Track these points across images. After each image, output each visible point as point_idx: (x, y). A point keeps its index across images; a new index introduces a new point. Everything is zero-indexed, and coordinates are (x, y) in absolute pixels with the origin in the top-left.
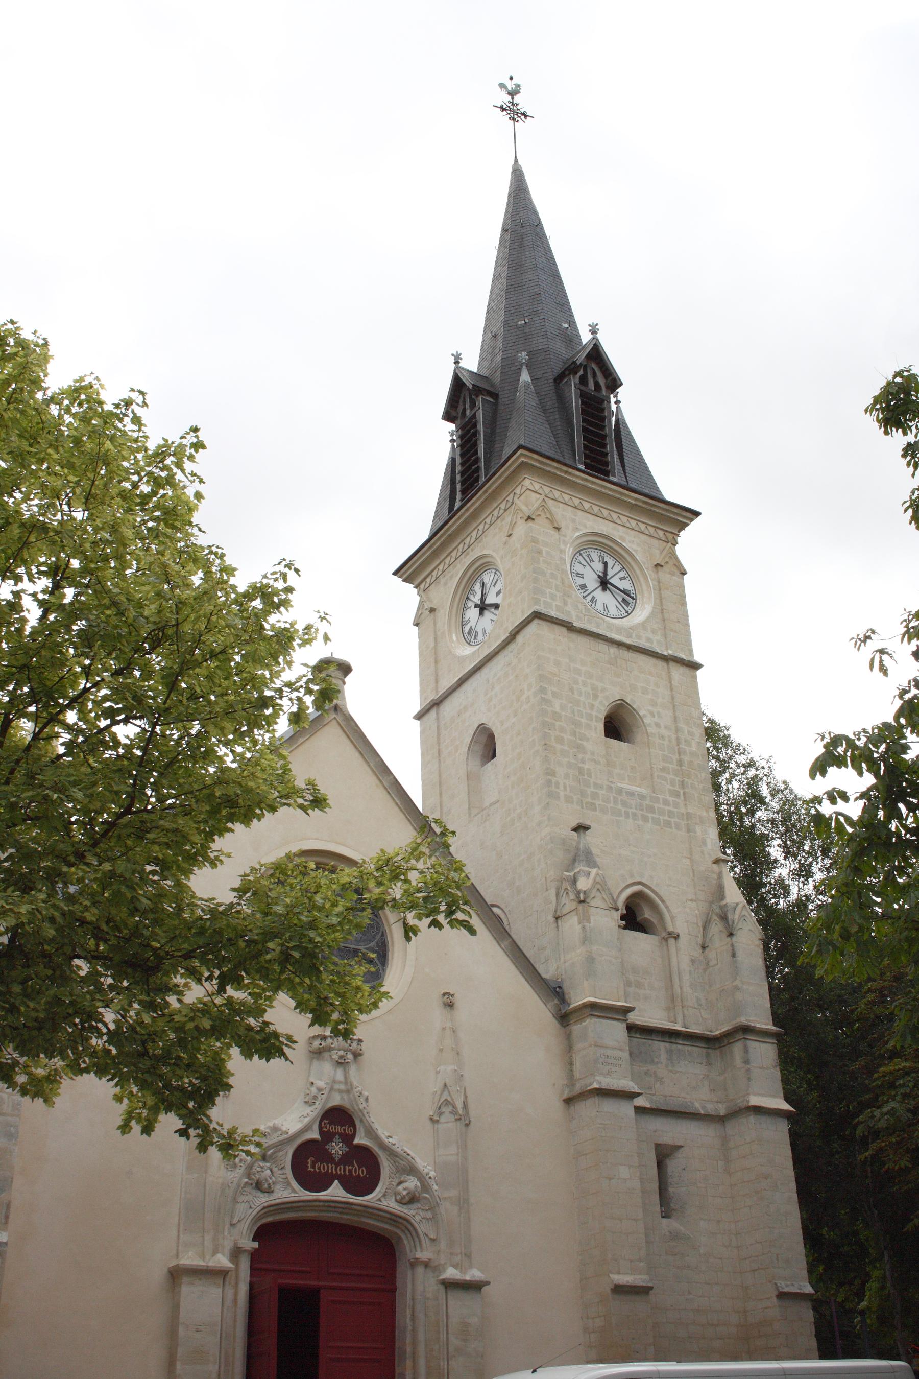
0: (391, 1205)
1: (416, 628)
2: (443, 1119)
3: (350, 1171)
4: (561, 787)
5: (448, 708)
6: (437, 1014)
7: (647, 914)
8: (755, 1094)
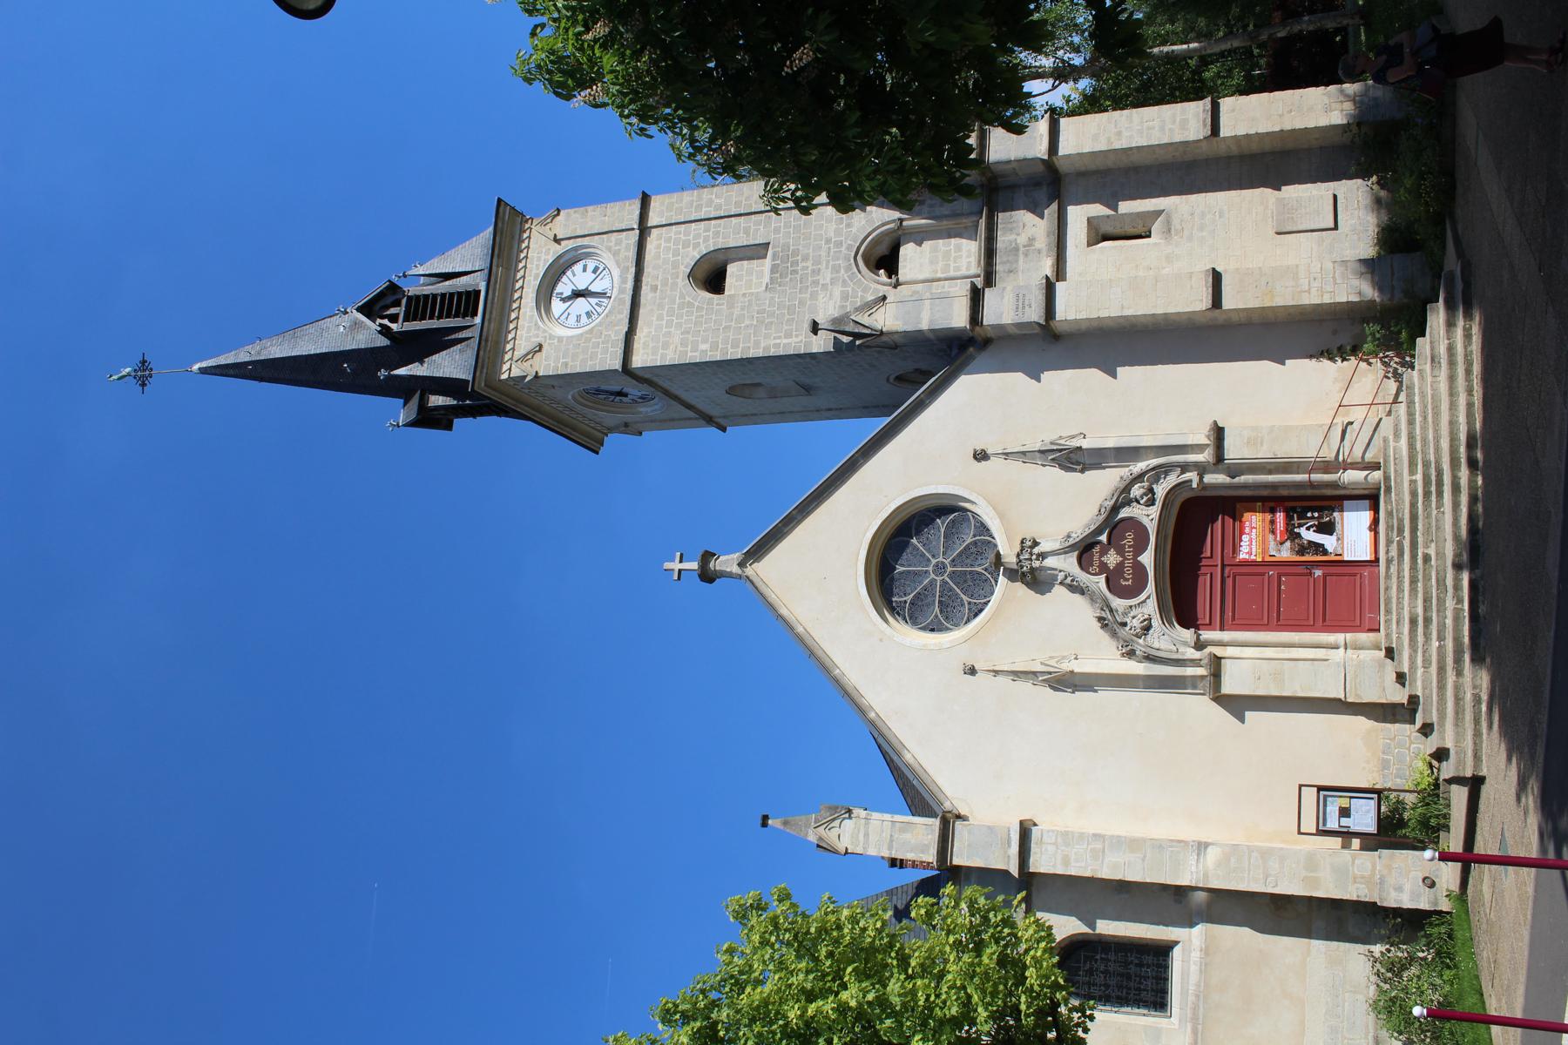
0: (1154, 511)
6: (994, 463)
7: (883, 249)
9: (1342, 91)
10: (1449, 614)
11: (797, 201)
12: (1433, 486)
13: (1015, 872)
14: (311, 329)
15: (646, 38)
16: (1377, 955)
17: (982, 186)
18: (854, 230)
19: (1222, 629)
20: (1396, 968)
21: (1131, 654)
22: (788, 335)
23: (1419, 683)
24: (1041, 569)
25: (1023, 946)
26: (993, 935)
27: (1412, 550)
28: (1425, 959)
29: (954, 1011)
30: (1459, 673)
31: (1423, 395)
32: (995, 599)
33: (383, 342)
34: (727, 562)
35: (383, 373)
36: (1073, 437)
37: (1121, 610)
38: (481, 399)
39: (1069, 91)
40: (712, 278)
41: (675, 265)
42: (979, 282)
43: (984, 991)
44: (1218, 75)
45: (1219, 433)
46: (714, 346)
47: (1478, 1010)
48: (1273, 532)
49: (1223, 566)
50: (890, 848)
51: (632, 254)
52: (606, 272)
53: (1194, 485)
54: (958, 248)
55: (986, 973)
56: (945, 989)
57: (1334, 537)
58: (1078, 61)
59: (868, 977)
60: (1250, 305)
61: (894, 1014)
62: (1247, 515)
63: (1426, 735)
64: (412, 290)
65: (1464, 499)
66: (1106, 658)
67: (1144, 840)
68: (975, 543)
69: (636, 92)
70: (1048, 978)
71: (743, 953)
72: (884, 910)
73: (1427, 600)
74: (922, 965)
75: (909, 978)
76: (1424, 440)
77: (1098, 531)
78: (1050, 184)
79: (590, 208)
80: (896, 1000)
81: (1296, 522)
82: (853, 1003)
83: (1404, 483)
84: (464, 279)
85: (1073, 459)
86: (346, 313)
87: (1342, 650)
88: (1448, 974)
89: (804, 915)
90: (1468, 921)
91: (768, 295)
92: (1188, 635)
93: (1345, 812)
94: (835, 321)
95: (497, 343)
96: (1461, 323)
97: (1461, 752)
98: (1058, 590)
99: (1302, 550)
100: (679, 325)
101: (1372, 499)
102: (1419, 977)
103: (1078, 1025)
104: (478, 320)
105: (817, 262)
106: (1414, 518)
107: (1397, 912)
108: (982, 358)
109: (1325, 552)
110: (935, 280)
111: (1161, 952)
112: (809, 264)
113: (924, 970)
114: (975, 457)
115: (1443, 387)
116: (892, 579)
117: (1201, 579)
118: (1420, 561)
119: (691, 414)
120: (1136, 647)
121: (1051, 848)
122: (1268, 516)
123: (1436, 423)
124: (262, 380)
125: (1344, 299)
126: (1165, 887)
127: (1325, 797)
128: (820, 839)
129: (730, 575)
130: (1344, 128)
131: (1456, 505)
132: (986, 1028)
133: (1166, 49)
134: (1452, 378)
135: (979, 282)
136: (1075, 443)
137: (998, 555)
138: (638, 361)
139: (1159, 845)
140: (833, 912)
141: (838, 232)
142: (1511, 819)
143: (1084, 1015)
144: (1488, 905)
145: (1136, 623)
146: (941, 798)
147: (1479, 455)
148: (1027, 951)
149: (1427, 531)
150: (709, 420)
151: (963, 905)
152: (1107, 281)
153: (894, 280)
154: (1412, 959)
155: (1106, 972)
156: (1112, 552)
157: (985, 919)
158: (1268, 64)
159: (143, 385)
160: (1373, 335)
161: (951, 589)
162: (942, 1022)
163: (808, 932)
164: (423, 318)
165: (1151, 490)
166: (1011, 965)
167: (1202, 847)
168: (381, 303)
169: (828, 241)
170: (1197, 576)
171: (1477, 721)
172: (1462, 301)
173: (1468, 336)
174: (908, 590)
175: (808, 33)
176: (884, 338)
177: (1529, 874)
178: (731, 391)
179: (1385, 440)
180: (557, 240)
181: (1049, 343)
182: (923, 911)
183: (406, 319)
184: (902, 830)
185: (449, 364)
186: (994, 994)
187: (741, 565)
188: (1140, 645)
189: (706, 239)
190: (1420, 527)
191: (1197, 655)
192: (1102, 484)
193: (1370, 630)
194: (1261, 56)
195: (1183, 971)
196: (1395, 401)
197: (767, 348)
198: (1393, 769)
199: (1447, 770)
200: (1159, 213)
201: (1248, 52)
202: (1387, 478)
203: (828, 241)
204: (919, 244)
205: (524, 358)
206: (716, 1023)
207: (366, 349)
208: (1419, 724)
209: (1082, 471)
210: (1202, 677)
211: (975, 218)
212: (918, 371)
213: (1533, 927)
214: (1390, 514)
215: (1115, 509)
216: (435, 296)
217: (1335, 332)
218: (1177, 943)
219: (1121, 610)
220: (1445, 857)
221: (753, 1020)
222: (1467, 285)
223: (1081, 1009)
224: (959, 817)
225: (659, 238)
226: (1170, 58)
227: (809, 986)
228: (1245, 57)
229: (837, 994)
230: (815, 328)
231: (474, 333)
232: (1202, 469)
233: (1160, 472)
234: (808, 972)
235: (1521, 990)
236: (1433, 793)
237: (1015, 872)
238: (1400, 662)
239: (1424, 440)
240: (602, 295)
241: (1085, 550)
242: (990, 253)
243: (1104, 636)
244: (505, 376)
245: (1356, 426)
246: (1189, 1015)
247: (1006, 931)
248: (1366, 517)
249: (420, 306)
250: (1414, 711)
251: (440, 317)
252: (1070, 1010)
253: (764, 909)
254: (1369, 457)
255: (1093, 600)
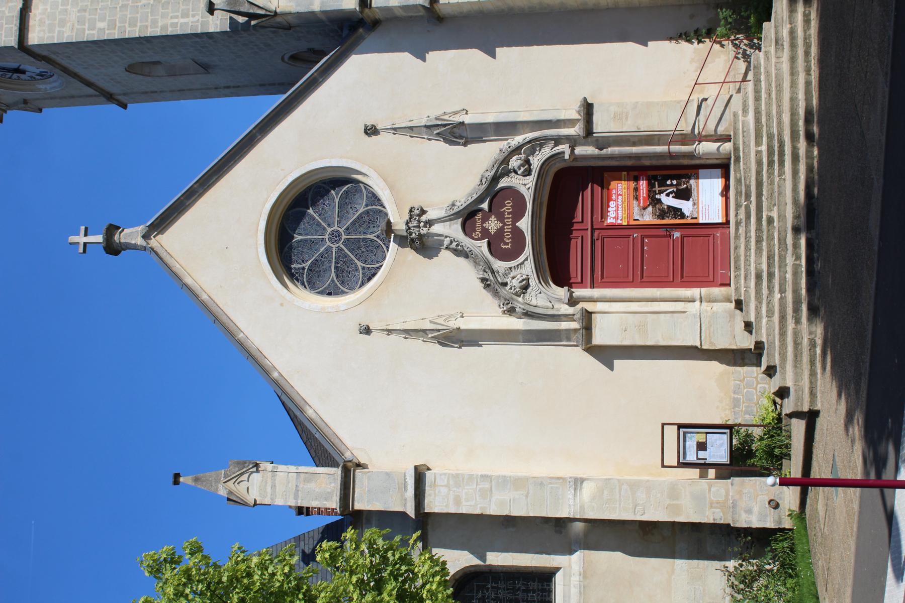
0: (531, 181)
1: (43, 110)
2: (464, 134)
3: (509, 214)
4: (176, 21)
6: (383, 138)
8: (576, 330)
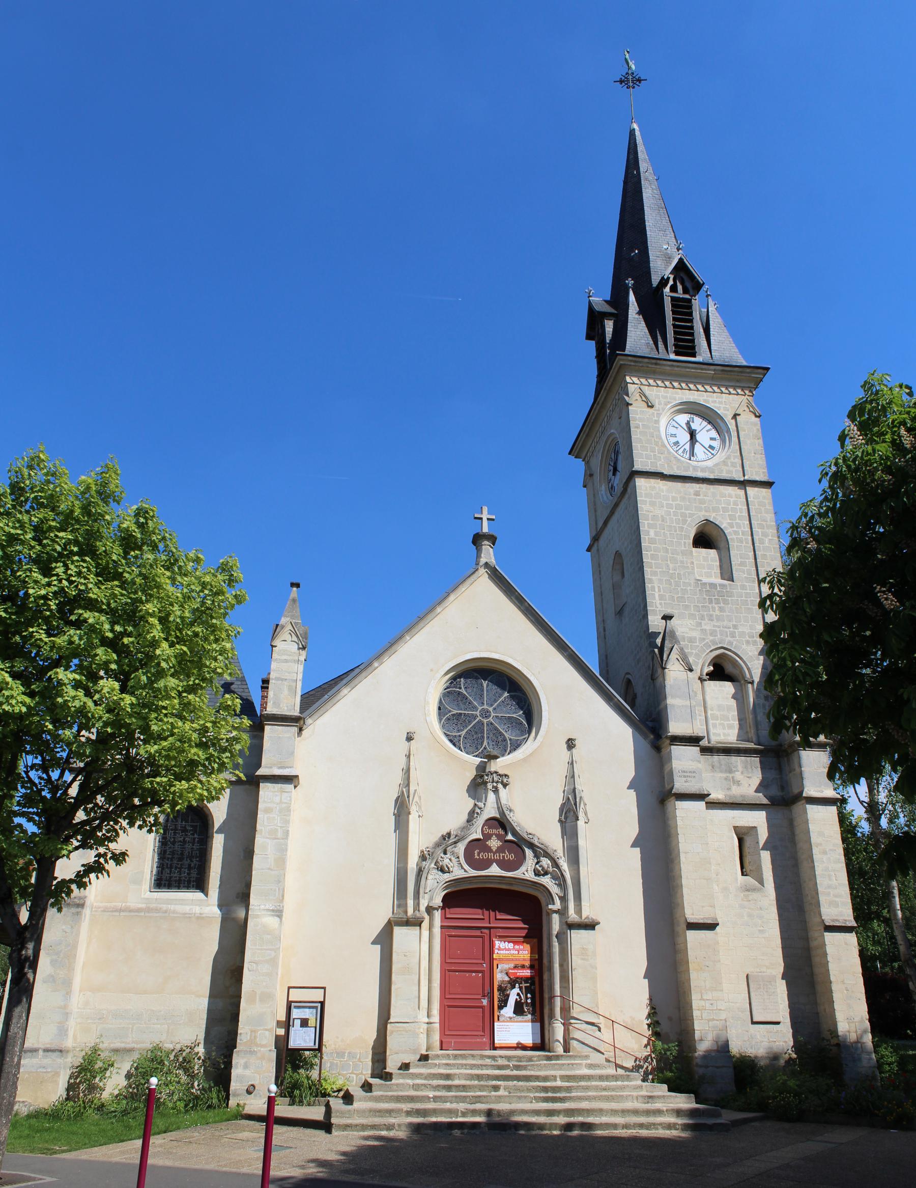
0: (530, 876)
5: (602, 541)
6: (565, 754)
7: (729, 669)
9: (865, 1032)
10: (454, 1106)
11: (770, 597)
12: (552, 1094)
13: (260, 772)
14: (665, 222)
15: (900, 475)
16: (196, 1050)
17: (781, 745)
18: (744, 646)
19: (442, 927)
20: (185, 1065)
21: (423, 858)
22: (661, 597)
23: (401, 1081)
24: (486, 790)
25: (204, 779)
26: (212, 756)
27: (500, 1077)
28: (193, 1087)
29: (154, 728)
30: (409, 1113)
31: (622, 1088)
32: (463, 755)
33: (655, 280)
34: (488, 554)
35: (630, 282)
36: (586, 814)
37: (456, 850)
38: (610, 360)
39: (857, 811)
40: (706, 538)
41: (715, 510)
42: (704, 743)
43: (170, 749)
44: (875, 934)
45: (590, 926)
46: (652, 541)
47: (154, 1129)
48: (516, 967)
49: (490, 928)
50: (277, 679)
51: (724, 475)
52: (711, 456)
53: (550, 907)
54: (730, 727)
55: (183, 751)
56: (171, 720)
57: (511, 1014)
58: (884, 822)
59: (180, 663)
60: (690, 953)
61: (151, 682)
62: (528, 947)
63: (363, 1087)
64: (696, 303)
65: (542, 1119)
66: (420, 838)
67: (284, 869)
68: (505, 740)
69: (857, 470)
70: (181, 797)
71: (196, 569)
72: (230, 674)
73: (464, 1088)
74: (189, 703)
75: (180, 694)
76: (587, 1088)
77: (515, 833)
78: (783, 798)
79: (761, 441)
80: (161, 684)
81: (524, 985)
82: (158, 652)
83: (553, 1071)
84: (704, 343)
85: (569, 814)
86: (678, 249)
87: (427, 1020)
88: (181, 1105)
89: (225, 614)
90: (221, 1121)
91: (692, 582)
92: (438, 901)
93: (304, 1023)
94: (673, 633)
95: (654, 372)
96: (680, 1121)
97: (350, 1114)
98: (470, 803)
99: (501, 989)
100: (669, 513)
101: (542, 1045)
102: (179, 1082)
103: (144, 821)
104: (672, 356)
105: (719, 619)
106: (527, 1078)
107: (229, 1065)
108: (645, 745)
109: (500, 1008)
110: (704, 709)
111: (200, 884)
112: (717, 612)
113: (185, 705)
114: (569, 740)
115: (629, 1105)
116: (477, 678)
117: (480, 911)
118: (494, 1083)
119: (600, 524)
120: (428, 861)
121: (277, 799)
122: (527, 964)
123: (600, 1098)
124: (625, 182)
125: (696, 1027)
126: (248, 885)
127: (316, 1008)
128: (283, 627)
129: (478, 556)
130: (834, 1032)
131: (537, 1112)
132: (142, 752)
133: (896, 892)
134: (636, 1112)
135: (704, 743)
136: (581, 815)
137: (496, 757)
138: (640, 482)
139: (280, 881)
140: (228, 636)
141: (742, 634)
142: (299, 1152)
143: (152, 826)
144: (233, 1136)
145: (446, 861)
146: (315, 716)
147: (575, 1133)
148: (200, 782)
149: (518, 1089)
150: (595, 539)
151: (234, 733)
152: (707, 841)
153: (705, 677)
154: (192, 1076)
155: (184, 842)
156: (500, 843)
157: (224, 750)
158: (886, 974)
159: (621, 82)
160: (668, 1050)
161: (470, 722)
162: (145, 719)
163: (212, 618)
164: (674, 312)
165: (546, 873)
166: (190, 770)
167: (278, 913)
168: (685, 278)
169: (735, 627)
170: (482, 909)
171: (374, 1127)
172: (698, 1123)
173: (670, 1126)
174: (469, 690)
175: (907, 604)
176: (659, 670)
177: (257, 1168)
178: (618, 555)
179: (587, 1057)
180: (735, 416)
181: (658, 797)
182: (229, 703)
183: (673, 299)
184: (290, 688)
185: (638, 335)
186: (168, 757)
187: (486, 565)
188: (430, 865)
189: (736, 533)
190: (521, 1083)
191: (423, 908)
192: (550, 835)
193: (441, 1042)
194: (892, 968)
195: (186, 901)
196: (617, 1066)
197: (651, 581)
198: (337, 1061)
199: (336, 1104)
200: (761, 882)
201: (895, 958)
202: (558, 1057)
203: (735, 627)
204: (734, 697)
205: (642, 394)
206: (140, 549)
207: (649, 268)
208: (371, 1081)
209: (560, 821)
210: (406, 912)
211: (754, 739)
212: (635, 697)
213: (217, 1172)
214: (530, 1059)
215: (532, 846)
216: (691, 321)
217: (670, 1019)
218: (206, 895)
219: (456, 850)
220: (271, 1101)
221: (145, 577)
222: (711, 1128)
223: (156, 823)
224: (301, 730)
225: (737, 496)
226: (888, 895)
227: (171, 619)
228: (891, 956)
229: (166, 639)
230: (667, 618)
231: (662, 354)
232: (563, 912)
233: (560, 880)
234: (182, 618)
235: (169, 1163)
236: (319, 1093)
237: (260, 772)
238: (418, 1066)
239: (587, 1088)
240: (692, 453)
241: (501, 823)
242: (727, 751)
243: (436, 837)
244: (628, 379)
245: (598, 1034)
246: (153, 906)
247: (216, 766)
248: (528, 1040)
249: (683, 309)
250: (381, 1078)
251: (674, 326)
252: (156, 815)
253: (229, 585)
254: (574, 1043)
255: (463, 829)
